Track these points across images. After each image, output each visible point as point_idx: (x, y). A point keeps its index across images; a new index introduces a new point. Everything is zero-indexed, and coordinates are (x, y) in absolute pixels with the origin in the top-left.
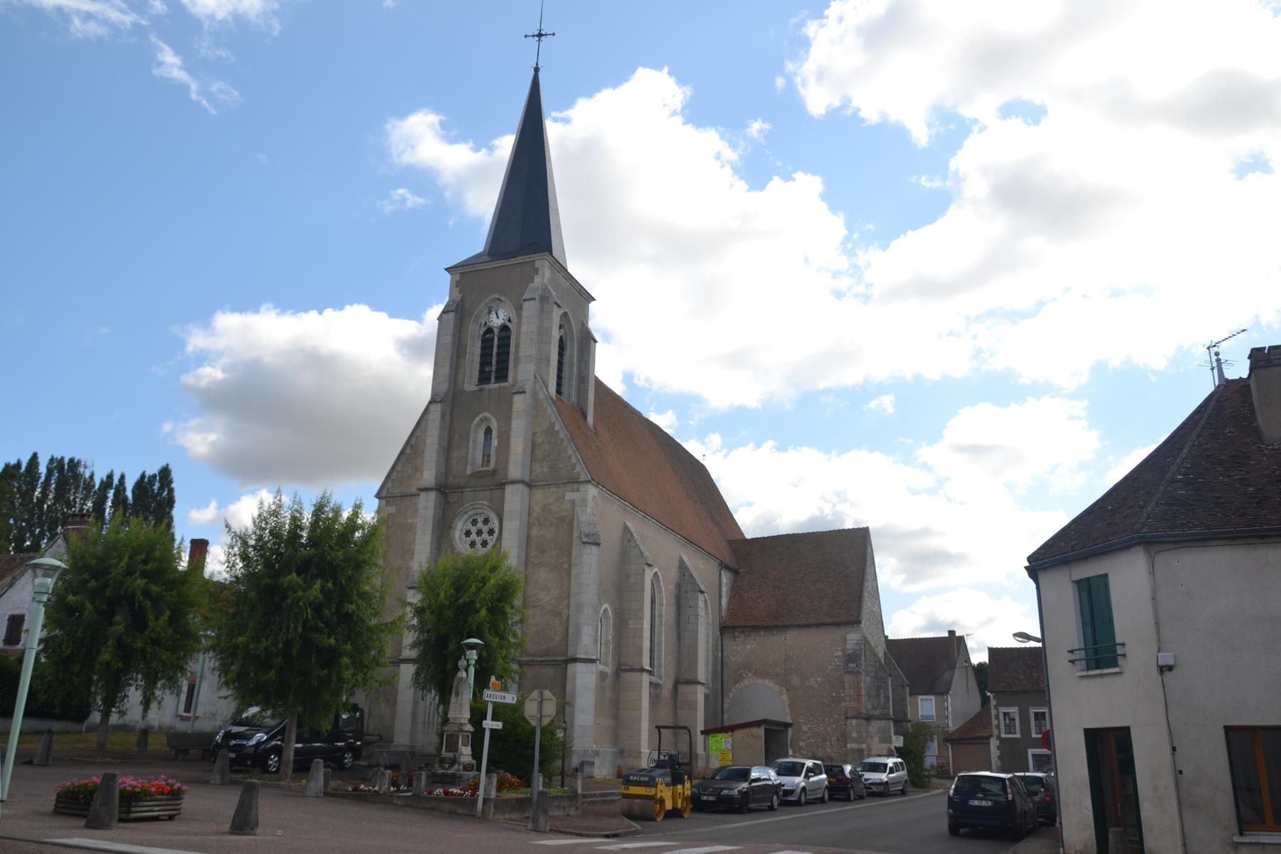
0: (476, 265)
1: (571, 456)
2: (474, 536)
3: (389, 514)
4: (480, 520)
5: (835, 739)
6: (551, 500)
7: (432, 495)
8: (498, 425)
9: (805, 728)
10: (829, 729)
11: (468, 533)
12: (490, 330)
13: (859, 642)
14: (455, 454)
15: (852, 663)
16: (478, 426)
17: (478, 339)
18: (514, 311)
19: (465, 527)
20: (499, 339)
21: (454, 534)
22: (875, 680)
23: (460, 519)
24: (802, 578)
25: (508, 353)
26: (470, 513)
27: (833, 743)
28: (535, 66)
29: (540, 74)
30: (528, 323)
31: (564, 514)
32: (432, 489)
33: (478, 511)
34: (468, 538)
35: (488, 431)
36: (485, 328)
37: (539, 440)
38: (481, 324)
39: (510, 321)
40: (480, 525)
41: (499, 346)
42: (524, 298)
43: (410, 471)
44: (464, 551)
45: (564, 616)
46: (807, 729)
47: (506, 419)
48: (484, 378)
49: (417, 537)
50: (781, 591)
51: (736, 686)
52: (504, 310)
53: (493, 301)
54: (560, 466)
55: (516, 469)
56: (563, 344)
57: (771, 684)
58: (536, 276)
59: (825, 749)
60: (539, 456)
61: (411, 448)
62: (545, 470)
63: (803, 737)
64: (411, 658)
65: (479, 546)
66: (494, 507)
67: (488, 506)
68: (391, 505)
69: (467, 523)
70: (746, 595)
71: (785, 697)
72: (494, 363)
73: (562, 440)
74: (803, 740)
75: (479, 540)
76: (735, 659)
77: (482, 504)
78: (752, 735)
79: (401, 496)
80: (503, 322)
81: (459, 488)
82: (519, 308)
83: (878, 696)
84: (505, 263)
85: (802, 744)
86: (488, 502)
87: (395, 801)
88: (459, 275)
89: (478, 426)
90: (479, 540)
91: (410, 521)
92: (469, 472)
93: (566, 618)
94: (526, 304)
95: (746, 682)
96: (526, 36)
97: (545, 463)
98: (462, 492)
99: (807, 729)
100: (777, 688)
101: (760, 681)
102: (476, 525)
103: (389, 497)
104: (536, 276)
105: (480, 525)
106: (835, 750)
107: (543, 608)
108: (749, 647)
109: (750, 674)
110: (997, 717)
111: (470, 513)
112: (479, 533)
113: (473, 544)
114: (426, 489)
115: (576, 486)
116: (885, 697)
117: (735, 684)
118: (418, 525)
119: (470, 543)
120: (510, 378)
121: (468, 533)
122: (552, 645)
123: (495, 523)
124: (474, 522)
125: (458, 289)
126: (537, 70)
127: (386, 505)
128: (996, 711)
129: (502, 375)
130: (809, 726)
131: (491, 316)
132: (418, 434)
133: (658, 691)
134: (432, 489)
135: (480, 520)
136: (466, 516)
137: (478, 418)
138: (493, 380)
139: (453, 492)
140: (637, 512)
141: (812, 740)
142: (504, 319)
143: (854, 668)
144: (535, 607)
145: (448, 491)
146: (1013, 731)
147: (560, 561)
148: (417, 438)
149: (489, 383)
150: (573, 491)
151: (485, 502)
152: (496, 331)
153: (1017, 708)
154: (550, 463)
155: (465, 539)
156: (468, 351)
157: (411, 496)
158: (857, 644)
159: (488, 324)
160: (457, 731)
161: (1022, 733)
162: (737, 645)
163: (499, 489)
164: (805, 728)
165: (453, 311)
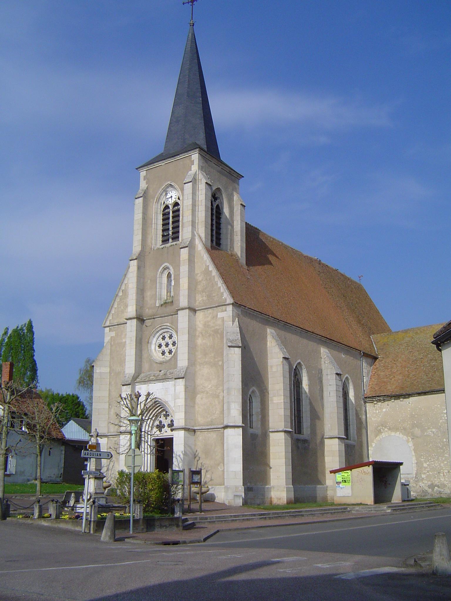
1: (220, 287)
2: (164, 347)
3: (111, 337)
4: (167, 335)
5: (446, 471)
6: (209, 319)
7: (135, 321)
9: (425, 465)
10: (442, 465)
11: (160, 346)
12: (167, 207)
17: (160, 214)
19: (158, 342)
23: (154, 337)
24: (421, 358)
26: (160, 332)
27: (445, 474)
31: (217, 327)
32: (134, 318)
33: (165, 330)
34: (160, 349)
35: (169, 276)
38: (161, 203)
39: (179, 199)
40: (167, 339)
42: (184, 182)
43: (122, 308)
44: (158, 358)
45: (221, 398)
46: (427, 466)
47: (177, 267)
48: (165, 241)
49: (127, 351)
50: (407, 369)
51: (377, 438)
54: (214, 295)
56: (219, 209)
57: (401, 435)
59: (440, 479)
62: (205, 298)
63: (424, 471)
65: (167, 354)
69: (159, 339)
70: (382, 373)
71: (411, 444)
72: (171, 229)
73: (214, 276)
74: (424, 473)
75: (167, 350)
76: (375, 419)
78: (364, 472)
80: (175, 200)
82: (182, 190)
85: (423, 476)
86: (170, 324)
89: (162, 273)
90: (167, 350)
91: (124, 340)
93: (222, 399)
95: (383, 435)
96: (183, 4)
97: (204, 294)
99: (427, 466)
100: (405, 438)
101: (393, 434)
102: (171, 339)
104: (192, 166)
105: (167, 339)
106: (447, 479)
107: (207, 393)
108: (384, 410)
109: (386, 429)
111: (160, 332)
113: (163, 353)
114: (130, 319)
115: (224, 307)
117: (376, 436)
119: (161, 352)
120: (180, 239)
122: (214, 418)
123: (175, 338)
124: (164, 338)
127: (110, 332)
129: (176, 237)
130: (428, 463)
132: (126, 282)
133: (307, 445)
134: (134, 318)
135: (167, 335)
136: (158, 334)
137: (162, 267)
140: (279, 322)
141: (431, 473)
142: (175, 198)
144: (203, 392)
147: (216, 360)
150: (222, 311)
151: (168, 324)
152: (171, 207)
155: (159, 350)
156: (153, 223)
159: (165, 203)
162: (376, 410)
164: (425, 465)
165: (141, 197)
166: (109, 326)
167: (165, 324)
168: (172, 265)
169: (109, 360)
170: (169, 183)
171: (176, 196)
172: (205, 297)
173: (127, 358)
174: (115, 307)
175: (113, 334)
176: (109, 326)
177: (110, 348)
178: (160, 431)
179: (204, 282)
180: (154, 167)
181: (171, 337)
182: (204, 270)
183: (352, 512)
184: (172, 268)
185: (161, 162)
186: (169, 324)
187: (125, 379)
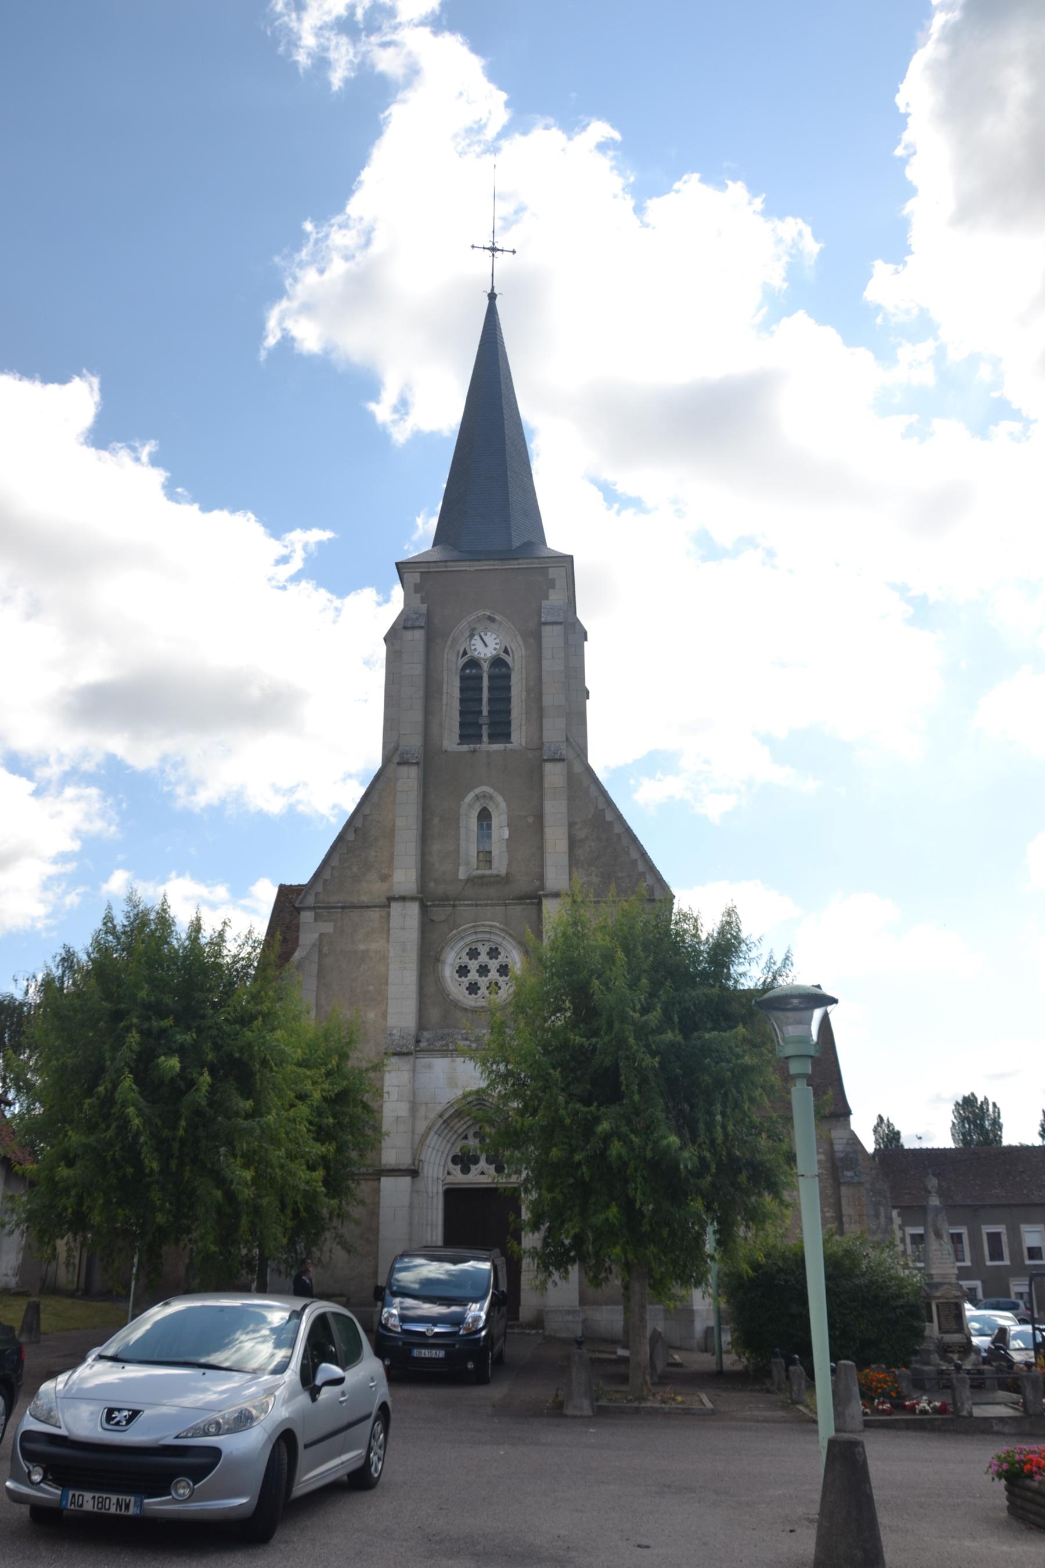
0: (449, 564)
2: (473, 975)
3: (321, 935)
4: (483, 950)
8: (508, 806)
13: (850, 1141)
14: (436, 847)
15: (848, 1170)
16: (471, 806)
18: (519, 638)
20: (490, 678)
21: (443, 970)
22: (871, 1194)
25: (508, 700)
26: (468, 940)
28: (489, 291)
29: (498, 302)
30: (553, 658)
32: (413, 899)
33: (480, 936)
35: (485, 816)
36: (465, 659)
37: (581, 834)
38: (459, 652)
39: (506, 651)
40: (483, 958)
41: (490, 689)
43: (355, 869)
52: (494, 636)
53: (479, 620)
55: (556, 876)
58: (551, 591)
60: (582, 858)
61: (355, 831)
64: (402, 1167)
66: (511, 932)
67: (502, 930)
68: (325, 921)
77: (491, 926)
79: (343, 908)
80: (494, 652)
81: (445, 900)
83: (877, 1216)
84: (498, 565)
87: (996, 1428)
88: (418, 574)
89: (471, 806)
92: (462, 875)
94: (546, 630)
98: (454, 906)
103: (319, 908)
104: (551, 591)
110: (903, 1240)
111: (468, 940)
112: (483, 970)
114: (403, 899)
116: (886, 1217)
118: (391, 954)
121: (463, 971)
124: (473, 954)
125: (419, 595)
126: (492, 297)
127: (316, 921)
128: (901, 1232)
129: (501, 731)
131: (473, 642)
132: (367, 812)
135: (483, 950)
136: (462, 943)
138: (485, 738)
139: (438, 906)
142: (495, 649)
143: (852, 1178)
145: (429, 903)
146: (960, 1257)
148: (365, 816)
149: (480, 742)
151: (498, 924)
152: (485, 666)
153: (1004, 1226)
154: (601, 870)
157: (362, 907)
158: (848, 1143)
160: (957, 1297)
161: (1012, 1260)
163: (521, 904)
165: (422, 627)
166: (314, 908)
167: (488, 923)
168: (503, 795)
169: (315, 989)
170: (488, 614)
171: (497, 644)
172: (596, 875)
173: (392, 990)
174: (333, 864)
175: (328, 928)
176: (314, 908)
177: (317, 960)
178: (466, 1170)
179: (592, 844)
180: (445, 569)
181: (493, 953)
182: (590, 816)
183: (801, 1408)
184: (502, 799)
185: (467, 563)
186: (498, 924)
187: (393, 1041)
